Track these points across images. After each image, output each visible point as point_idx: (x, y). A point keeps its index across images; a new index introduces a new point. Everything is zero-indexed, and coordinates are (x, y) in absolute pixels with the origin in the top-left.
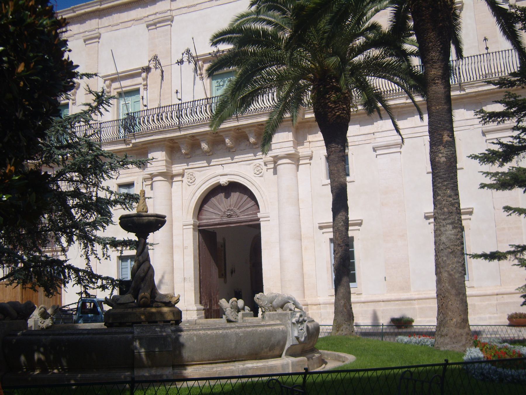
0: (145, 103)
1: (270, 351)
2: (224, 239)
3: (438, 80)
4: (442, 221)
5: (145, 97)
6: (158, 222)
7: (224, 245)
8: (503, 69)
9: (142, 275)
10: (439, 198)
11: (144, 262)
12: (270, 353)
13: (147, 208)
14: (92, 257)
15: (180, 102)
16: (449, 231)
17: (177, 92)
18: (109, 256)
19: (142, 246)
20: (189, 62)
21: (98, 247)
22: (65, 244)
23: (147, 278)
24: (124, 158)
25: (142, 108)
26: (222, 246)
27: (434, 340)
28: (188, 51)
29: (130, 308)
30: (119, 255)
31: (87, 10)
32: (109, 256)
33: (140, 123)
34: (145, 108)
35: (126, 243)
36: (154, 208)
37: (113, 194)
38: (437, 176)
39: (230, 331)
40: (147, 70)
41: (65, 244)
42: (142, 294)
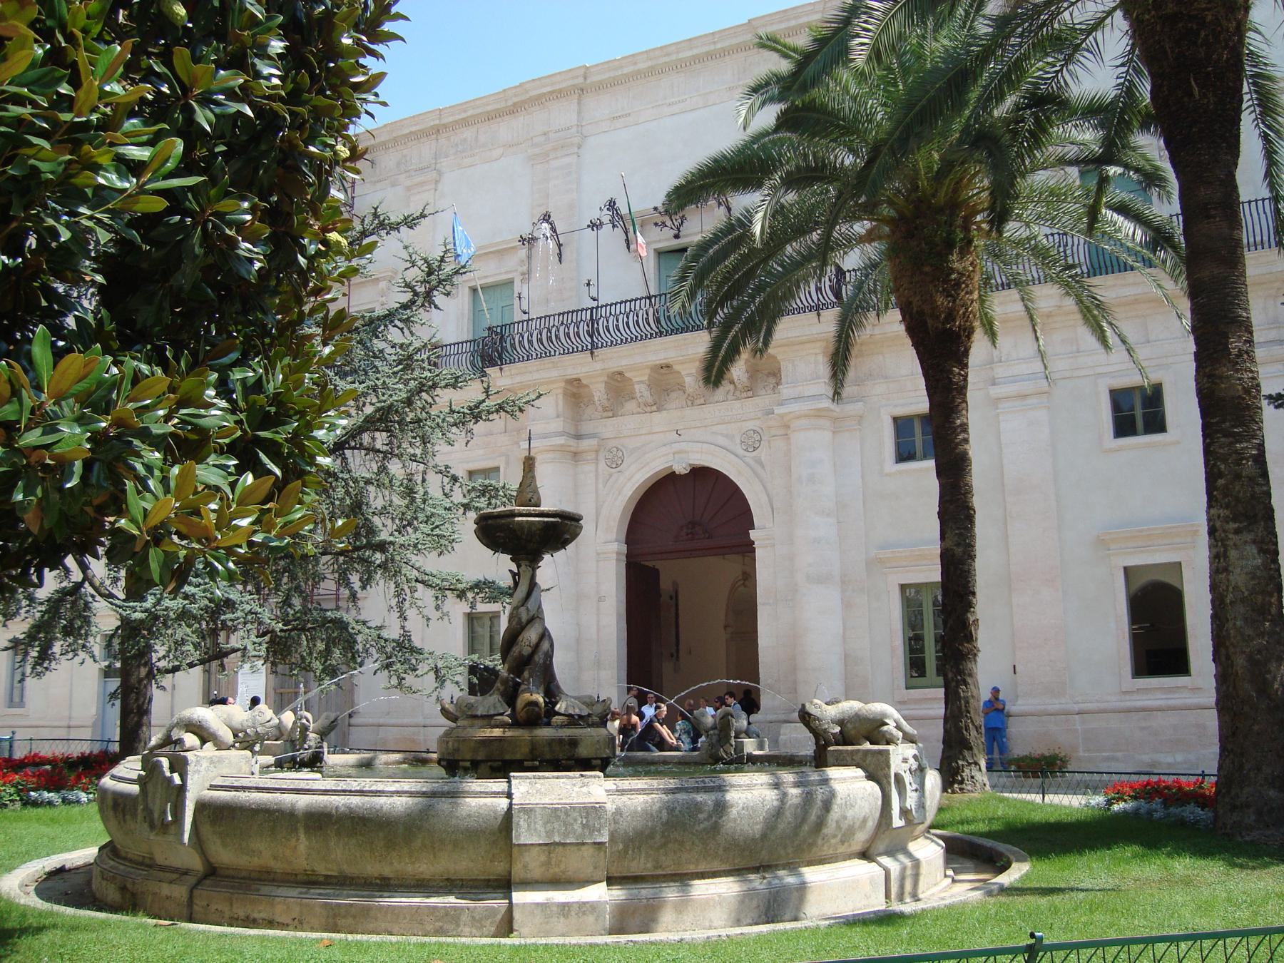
0: (526, 308)
1: (842, 842)
2: (675, 584)
3: (1215, 209)
4: (1231, 536)
5: (524, 294)
6: (560, 531)
7: (675, 596)
8: (1266, 238)
9: (527, 651)
10: (1221, 482)
11: (531, 620)
12: (842, 849)
13: (539, 499)
14: (411, 613)
15: (595, 304)
16: (1246, 558)
17: (588, 284)
18: (447, 614)
19: (526, 590)
20: (614, 226)
21: (425, 596)
22: (357, 585)
23: (536, 658)
24: (484, 396)
25: (519, 316)
26: (671, 598)
27: (1211, 814)
28: (612, 205)
29: (497, 727)
30: (469, 610)
31: (417, 900)
32: (447, 614)
33: (513, 346)
34: (525, 317)
35: (484, 588)
36: (553, 497)
37: (458, 484)
38: (1217, 432)
39: (749, 796)
40: (529, 241)
41: (357, 585)
42: (525, 697)
